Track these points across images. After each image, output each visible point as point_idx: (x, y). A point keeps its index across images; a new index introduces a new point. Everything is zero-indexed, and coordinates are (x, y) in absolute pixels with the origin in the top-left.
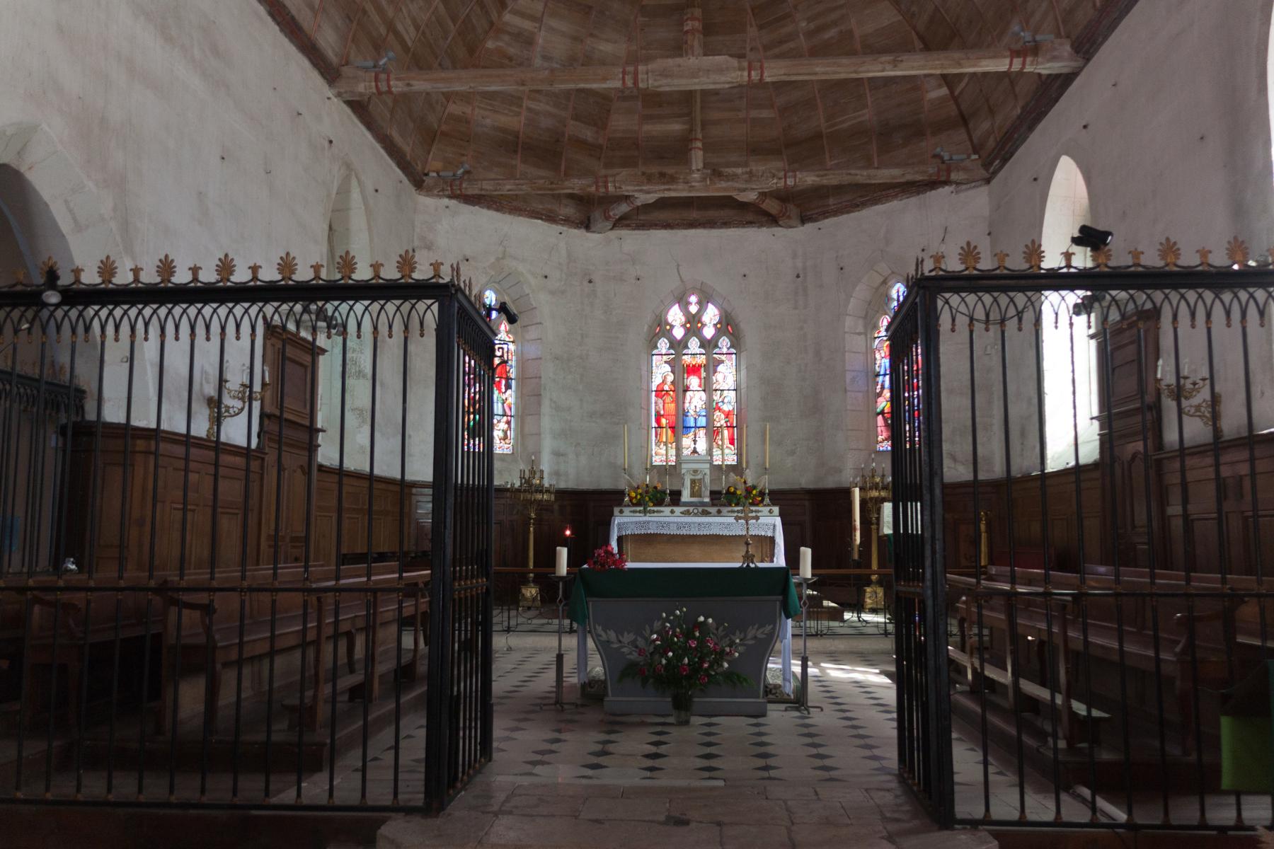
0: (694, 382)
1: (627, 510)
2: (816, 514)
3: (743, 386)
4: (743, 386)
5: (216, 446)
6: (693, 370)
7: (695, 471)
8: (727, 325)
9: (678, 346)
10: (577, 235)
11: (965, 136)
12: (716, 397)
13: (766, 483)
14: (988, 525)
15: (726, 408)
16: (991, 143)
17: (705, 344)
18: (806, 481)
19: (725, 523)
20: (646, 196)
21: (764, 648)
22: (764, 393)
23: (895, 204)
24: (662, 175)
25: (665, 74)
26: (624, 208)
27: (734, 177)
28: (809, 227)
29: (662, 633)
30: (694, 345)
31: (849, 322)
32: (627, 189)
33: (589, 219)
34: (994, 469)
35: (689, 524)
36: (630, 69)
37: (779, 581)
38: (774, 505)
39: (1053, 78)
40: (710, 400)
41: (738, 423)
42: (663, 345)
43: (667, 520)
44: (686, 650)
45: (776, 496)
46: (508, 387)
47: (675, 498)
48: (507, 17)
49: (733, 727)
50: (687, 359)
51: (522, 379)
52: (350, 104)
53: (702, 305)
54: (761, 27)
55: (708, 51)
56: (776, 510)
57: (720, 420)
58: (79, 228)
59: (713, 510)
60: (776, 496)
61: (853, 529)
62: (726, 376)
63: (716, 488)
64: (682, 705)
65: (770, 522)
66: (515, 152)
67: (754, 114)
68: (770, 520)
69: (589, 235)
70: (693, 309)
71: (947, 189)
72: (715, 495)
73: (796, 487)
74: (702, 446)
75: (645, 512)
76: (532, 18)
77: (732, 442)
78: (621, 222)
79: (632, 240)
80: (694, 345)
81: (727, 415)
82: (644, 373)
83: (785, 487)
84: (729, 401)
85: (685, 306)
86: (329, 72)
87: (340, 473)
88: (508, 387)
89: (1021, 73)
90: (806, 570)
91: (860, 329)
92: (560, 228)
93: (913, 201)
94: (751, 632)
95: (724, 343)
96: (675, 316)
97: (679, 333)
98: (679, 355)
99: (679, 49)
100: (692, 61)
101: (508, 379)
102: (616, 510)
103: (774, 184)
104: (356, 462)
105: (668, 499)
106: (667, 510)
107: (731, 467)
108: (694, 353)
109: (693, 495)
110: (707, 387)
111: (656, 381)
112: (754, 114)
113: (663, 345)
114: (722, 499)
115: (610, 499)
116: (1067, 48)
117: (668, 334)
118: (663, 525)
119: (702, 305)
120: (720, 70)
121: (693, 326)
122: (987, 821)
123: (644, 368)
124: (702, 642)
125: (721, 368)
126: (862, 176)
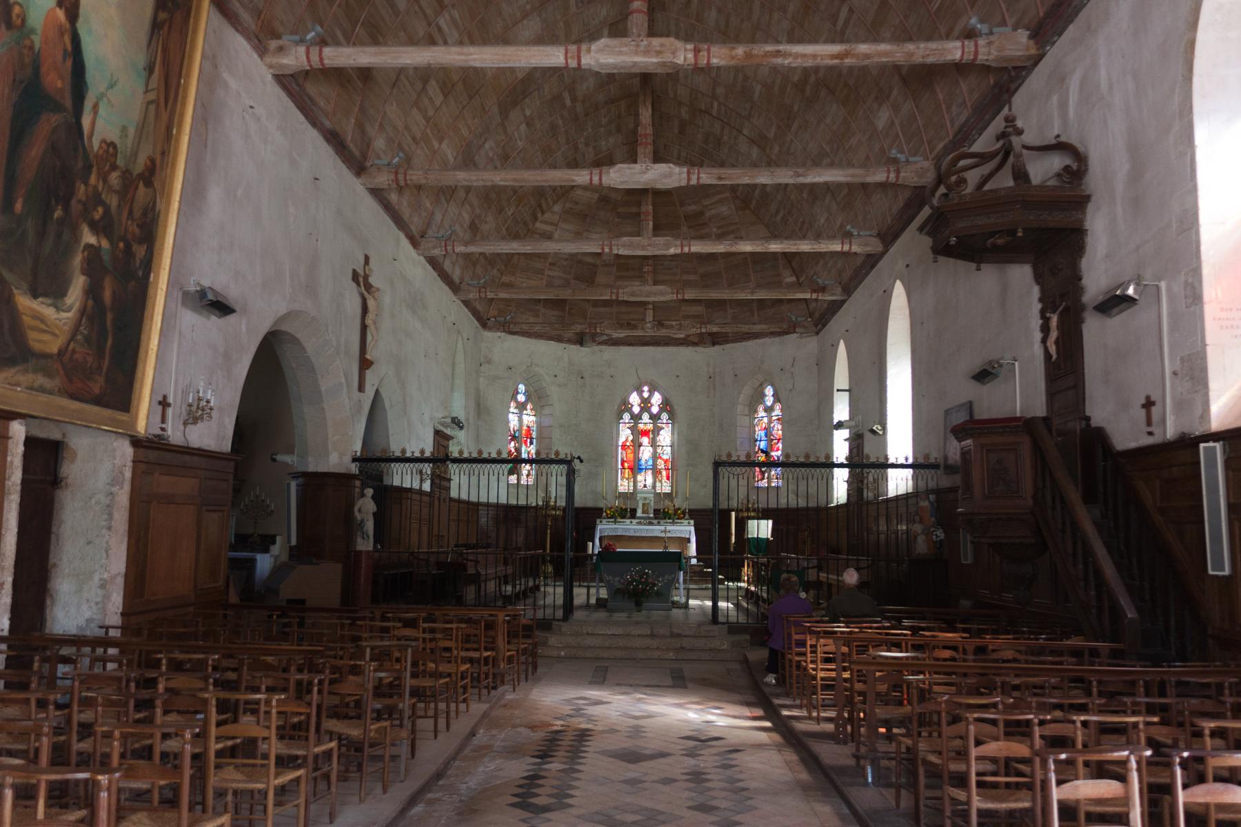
0: (645, 440)
1: (604, 521)
2: (713, 523)
5: (420, 492)
6: (645, 433)
8: (666, 406)
9: (636, 418)
12: (659, 450)
15: (665, 457)
16: (817, 315)
17: (652, 417)
22: (687, 447)
23: (767, 340)
26: (605, 338)
28: (717, 347)
30: (646, 417)
31: (740, 408)
32: (607, 332)
39: (834, 302)
41: (673, 466)
42: (626, 417)
43: (628, 527)
44: (641, 583)
46: (531, 443)
48: (538, 225)
49: (656, 614)
50: (641, 426)
51: (540, 438)
52: (463, 302)
53: (651, 392)
54: (690, 227)
55: (655, 283)
56: (692, 522)
57: (661, 465)
58: (392, 406)
59: (655, 522)
61: (730, 534)
62: (665, 437)
64: (638, 605)
65: (687, 529)
67: (685, 277)
68: (687, 528)
70: (646, 395)
72: (656, 511)
74: (650, 481)
75: (615, 522)
76: (552, 224)
79: (609, 352)
80: (646, 417)
81: (666, 461)
83: (699, 507)
84: (667, 453)
85: (640, 393)
86: (455, 288)
87: (459, 501)
88: (531, 443)
92: (567, 345)
93: (777, 339)
95: (665, 416)
96: (634, 399)
97: (636, 410)
98: (636, 424)
100: (648, 288)
101: (531, 439)
103: (694, 331)
104: (464, 496)
108: (646, 422)
110: (654, 444)
111: (622, 440)
112: (685, 277)
113: (626, 417)
114: (661, 515)
115: (595, 513)
117: (630, 410)
119: (651, 392)
120: (662, 294)
121: (646, 404)
126: (745, 328)
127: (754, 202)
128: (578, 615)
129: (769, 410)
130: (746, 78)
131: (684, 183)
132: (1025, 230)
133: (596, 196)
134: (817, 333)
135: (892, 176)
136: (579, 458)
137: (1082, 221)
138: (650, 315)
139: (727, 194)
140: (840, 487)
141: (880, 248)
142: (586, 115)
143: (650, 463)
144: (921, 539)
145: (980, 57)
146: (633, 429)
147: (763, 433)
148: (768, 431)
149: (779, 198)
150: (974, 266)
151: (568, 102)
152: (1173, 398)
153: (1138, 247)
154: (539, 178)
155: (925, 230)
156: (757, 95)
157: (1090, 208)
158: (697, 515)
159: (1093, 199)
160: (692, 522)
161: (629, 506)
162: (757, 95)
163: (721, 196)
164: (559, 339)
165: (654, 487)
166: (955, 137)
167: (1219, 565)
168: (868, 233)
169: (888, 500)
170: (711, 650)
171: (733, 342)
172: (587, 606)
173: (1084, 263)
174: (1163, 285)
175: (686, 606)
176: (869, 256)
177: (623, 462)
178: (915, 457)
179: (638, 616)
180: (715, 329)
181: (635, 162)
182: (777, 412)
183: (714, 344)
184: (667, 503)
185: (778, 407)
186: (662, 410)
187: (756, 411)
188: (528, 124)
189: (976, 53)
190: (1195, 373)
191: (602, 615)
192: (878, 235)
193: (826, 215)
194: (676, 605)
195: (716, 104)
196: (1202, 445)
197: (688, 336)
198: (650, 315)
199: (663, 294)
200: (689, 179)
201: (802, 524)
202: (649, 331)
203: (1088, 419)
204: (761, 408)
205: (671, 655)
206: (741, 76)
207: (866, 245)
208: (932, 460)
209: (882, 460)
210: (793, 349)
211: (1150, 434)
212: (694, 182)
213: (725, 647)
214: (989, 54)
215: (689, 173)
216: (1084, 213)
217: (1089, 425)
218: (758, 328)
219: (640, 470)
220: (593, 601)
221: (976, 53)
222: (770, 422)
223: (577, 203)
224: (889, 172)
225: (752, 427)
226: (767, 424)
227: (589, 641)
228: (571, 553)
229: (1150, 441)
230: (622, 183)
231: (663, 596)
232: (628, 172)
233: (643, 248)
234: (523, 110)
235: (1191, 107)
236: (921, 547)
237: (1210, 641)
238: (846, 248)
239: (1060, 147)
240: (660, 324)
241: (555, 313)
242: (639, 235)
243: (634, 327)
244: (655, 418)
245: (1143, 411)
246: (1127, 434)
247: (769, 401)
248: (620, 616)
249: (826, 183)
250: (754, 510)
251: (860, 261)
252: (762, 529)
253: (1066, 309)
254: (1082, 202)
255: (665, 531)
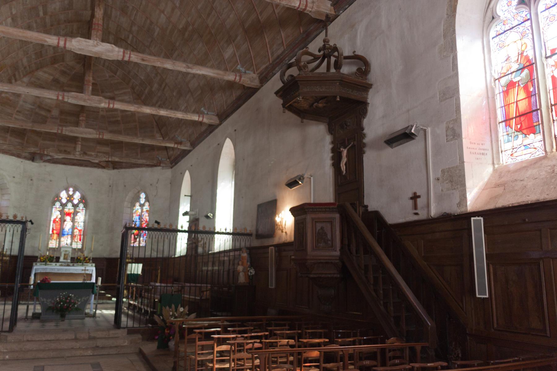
0: (68, 218)
1: (38, 264)
3: (86, 223)
4: (87, 221)
6: (69, 214)
7: (66, 251)
8: (83, 200)
9: (64, 205)
10: (28, 163)
11: (166, 153)
12: (76, 224)
13: (91, 256)
14: (161, 271)
15: (79, 228)
16: (173, 158)
18: (106, 255)
19: (78, 269)
20: (60, 156)
21: (87, 302)
23: (144, 169)
24: (65, 151)
25: (72, 131)
26: (49, 158)
27: (91, 155)
28: (116, 171)
29: (60, 298)
30: (70, 205)
31: (126, 203)
32: (51, 154)
33: (34, 158)
34: (166, 254)
35: (62, 269)
36: (60, 128)
37: (92, 286)
38: (93, 263)
39: (184, 150)
40: (73, 225)
41: (84, 234)
42: (58, 204)
43: (53, 267)
44: (66, 302)
45: (95, 260)
47: (58, 260)
49: (76, 323)
50: (66, 210)
53: (74, 192)
55: (86, 127)
56: (94, 265)
57: (76, 232)
59: (71, 264)
60: (95, 260)
63: (73, 256)
64: (63, 316)
65: (91, 269)
66: (8, 132)
69: (33, 163)
71: (160, 168)
73: (102, 257)
74: (69, 241)
75: (46, 264)
77: (80, 240)
78: (49, 161)
79: (50, 167)
80: (70, 205)
81: (80, 231)
82: (49, 214)
83: (98, 256)
85: (67, 191)
89: (177, 148)
90: (99, 283)
91: (129, 206)
92: (23, 160)
93: (150, 169)
94: (83, 298)
96: (63, 195)
97: (64, 201)
98: (63, 208)
99: (77, 124)
100: (81, 129)
102: (34, 264)
103: (104, 159)
105: (55, 260)
106: (54, 264)
107: (79, 249)
108: (69, 208)
109: (64, 259)
110: (73, 220)
114: (75, 260)
115: (33, 259)
116: (189, 144)
117: (60, 201)
118: (52, 269)
119: (74, 192)
120: (90, 133)
121: (70, 198)
122: (127, 327)
123: (49, 212)
124: (70, 300)
125: (79, 214)
126: (133, 161)
127: (144, 96)
128: (20, 325)
129: (142, 206)
130: (151, 23)
131: (120, 58)
132: (340, 97)
133: (52, 78)
134: (172, 168)
135: (238, 78)
136: (31, 221)
137: (367, 98)
138: (79, 148)
139: (129, 90)
140: (182, 244)
141: (217, 122)
142: (52, 25)
143: (71, 231)
144: (242, 275)
145: (308, 8)
146: (61, 212)
147: (137, 217)
148: (141, 217)
149: (159, 94)
150: (299, 119)
151: (41, 14)
152: (435, 193)
153: (408, 111)
154: (20, 34)
155: (280, 94)
156: (156, 34)
157: (371, 92)
158: (96, 261)
159: (373, 87)
160: (94, 265)
161: (56, 255)
162: (156, 34)
163: (125, 91)
164: (18, 156)
165: (71, 244)
166: (273, 62)
167: (482, 292)
168: (213, 113)
169: (214, 254)
170: (116, 347)
171: (125, 168)
172: (26, 318)
173: (365, 122)
174: (429, 130)
175: (94, 315)
176: (210, 125)
177: (53, 230)
178: (234, 228)
179: (64, 325)
180: (117, 159)
181: (90, 39)
182: (146, 207)
183: (114, 168)
184: (80, 253)
185: (147, 204)
186: (80, 202)
187: (134, 206)
188: (13, 19)
189: (306, 6)
190: (456, 178)
191: (36, 325)
192: (217, 115)
193: (185, 105)
194: (88, 315)
195: (131, 36)
196: (472, 219)
197: (100, 162)
198: (79, 148)
199: (91, 134)
200: (124, 56)
201: (160, 266)
202: (77, 156)
203: (366, 207)
204: (137, 204)
205: (90, 352)
206: (148, 21)
207: (211, 119)
208: (248, 232)
209: (212, 230)
210: (161, 174)
211: (416, 214)
212: (126, 59)
213: (126, 344)
214: (312, 8)
215: (124, 53)
216: (367, 94)
217: (367, 210)
218: (140, 161)
219: (63, 235)
220: (30, 314)
221: (306, 6)
222: (142, 211)
223: (39, 79)
224: (236, 76)
225: (132, 214)
226: (141, 212)
227: (29, 346)
228: (19, 285)
229: (416, 218)
230: (80, 49)
231: (80, 310)
232: (85, 43)
233: (85, 100)
234: (11, 9)
235: (454, 31)
236: (242, 279)
237: (468, 338)
238: (201, 119)
239: (356, 57)
240: (85, 154)
241: (17, 140)
242: (82, 93)
243: (69, 153)
244: (75, 206)
245: (411, 202)
246: (396, 213)
247: (142, 201)
248: (50, 326)
249: (203, 75)
250: (131, 259)
251: (203, 128)
252: (136, 269)
253: (354, 146)
254: (367, 87)
255: (85, 270)
